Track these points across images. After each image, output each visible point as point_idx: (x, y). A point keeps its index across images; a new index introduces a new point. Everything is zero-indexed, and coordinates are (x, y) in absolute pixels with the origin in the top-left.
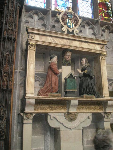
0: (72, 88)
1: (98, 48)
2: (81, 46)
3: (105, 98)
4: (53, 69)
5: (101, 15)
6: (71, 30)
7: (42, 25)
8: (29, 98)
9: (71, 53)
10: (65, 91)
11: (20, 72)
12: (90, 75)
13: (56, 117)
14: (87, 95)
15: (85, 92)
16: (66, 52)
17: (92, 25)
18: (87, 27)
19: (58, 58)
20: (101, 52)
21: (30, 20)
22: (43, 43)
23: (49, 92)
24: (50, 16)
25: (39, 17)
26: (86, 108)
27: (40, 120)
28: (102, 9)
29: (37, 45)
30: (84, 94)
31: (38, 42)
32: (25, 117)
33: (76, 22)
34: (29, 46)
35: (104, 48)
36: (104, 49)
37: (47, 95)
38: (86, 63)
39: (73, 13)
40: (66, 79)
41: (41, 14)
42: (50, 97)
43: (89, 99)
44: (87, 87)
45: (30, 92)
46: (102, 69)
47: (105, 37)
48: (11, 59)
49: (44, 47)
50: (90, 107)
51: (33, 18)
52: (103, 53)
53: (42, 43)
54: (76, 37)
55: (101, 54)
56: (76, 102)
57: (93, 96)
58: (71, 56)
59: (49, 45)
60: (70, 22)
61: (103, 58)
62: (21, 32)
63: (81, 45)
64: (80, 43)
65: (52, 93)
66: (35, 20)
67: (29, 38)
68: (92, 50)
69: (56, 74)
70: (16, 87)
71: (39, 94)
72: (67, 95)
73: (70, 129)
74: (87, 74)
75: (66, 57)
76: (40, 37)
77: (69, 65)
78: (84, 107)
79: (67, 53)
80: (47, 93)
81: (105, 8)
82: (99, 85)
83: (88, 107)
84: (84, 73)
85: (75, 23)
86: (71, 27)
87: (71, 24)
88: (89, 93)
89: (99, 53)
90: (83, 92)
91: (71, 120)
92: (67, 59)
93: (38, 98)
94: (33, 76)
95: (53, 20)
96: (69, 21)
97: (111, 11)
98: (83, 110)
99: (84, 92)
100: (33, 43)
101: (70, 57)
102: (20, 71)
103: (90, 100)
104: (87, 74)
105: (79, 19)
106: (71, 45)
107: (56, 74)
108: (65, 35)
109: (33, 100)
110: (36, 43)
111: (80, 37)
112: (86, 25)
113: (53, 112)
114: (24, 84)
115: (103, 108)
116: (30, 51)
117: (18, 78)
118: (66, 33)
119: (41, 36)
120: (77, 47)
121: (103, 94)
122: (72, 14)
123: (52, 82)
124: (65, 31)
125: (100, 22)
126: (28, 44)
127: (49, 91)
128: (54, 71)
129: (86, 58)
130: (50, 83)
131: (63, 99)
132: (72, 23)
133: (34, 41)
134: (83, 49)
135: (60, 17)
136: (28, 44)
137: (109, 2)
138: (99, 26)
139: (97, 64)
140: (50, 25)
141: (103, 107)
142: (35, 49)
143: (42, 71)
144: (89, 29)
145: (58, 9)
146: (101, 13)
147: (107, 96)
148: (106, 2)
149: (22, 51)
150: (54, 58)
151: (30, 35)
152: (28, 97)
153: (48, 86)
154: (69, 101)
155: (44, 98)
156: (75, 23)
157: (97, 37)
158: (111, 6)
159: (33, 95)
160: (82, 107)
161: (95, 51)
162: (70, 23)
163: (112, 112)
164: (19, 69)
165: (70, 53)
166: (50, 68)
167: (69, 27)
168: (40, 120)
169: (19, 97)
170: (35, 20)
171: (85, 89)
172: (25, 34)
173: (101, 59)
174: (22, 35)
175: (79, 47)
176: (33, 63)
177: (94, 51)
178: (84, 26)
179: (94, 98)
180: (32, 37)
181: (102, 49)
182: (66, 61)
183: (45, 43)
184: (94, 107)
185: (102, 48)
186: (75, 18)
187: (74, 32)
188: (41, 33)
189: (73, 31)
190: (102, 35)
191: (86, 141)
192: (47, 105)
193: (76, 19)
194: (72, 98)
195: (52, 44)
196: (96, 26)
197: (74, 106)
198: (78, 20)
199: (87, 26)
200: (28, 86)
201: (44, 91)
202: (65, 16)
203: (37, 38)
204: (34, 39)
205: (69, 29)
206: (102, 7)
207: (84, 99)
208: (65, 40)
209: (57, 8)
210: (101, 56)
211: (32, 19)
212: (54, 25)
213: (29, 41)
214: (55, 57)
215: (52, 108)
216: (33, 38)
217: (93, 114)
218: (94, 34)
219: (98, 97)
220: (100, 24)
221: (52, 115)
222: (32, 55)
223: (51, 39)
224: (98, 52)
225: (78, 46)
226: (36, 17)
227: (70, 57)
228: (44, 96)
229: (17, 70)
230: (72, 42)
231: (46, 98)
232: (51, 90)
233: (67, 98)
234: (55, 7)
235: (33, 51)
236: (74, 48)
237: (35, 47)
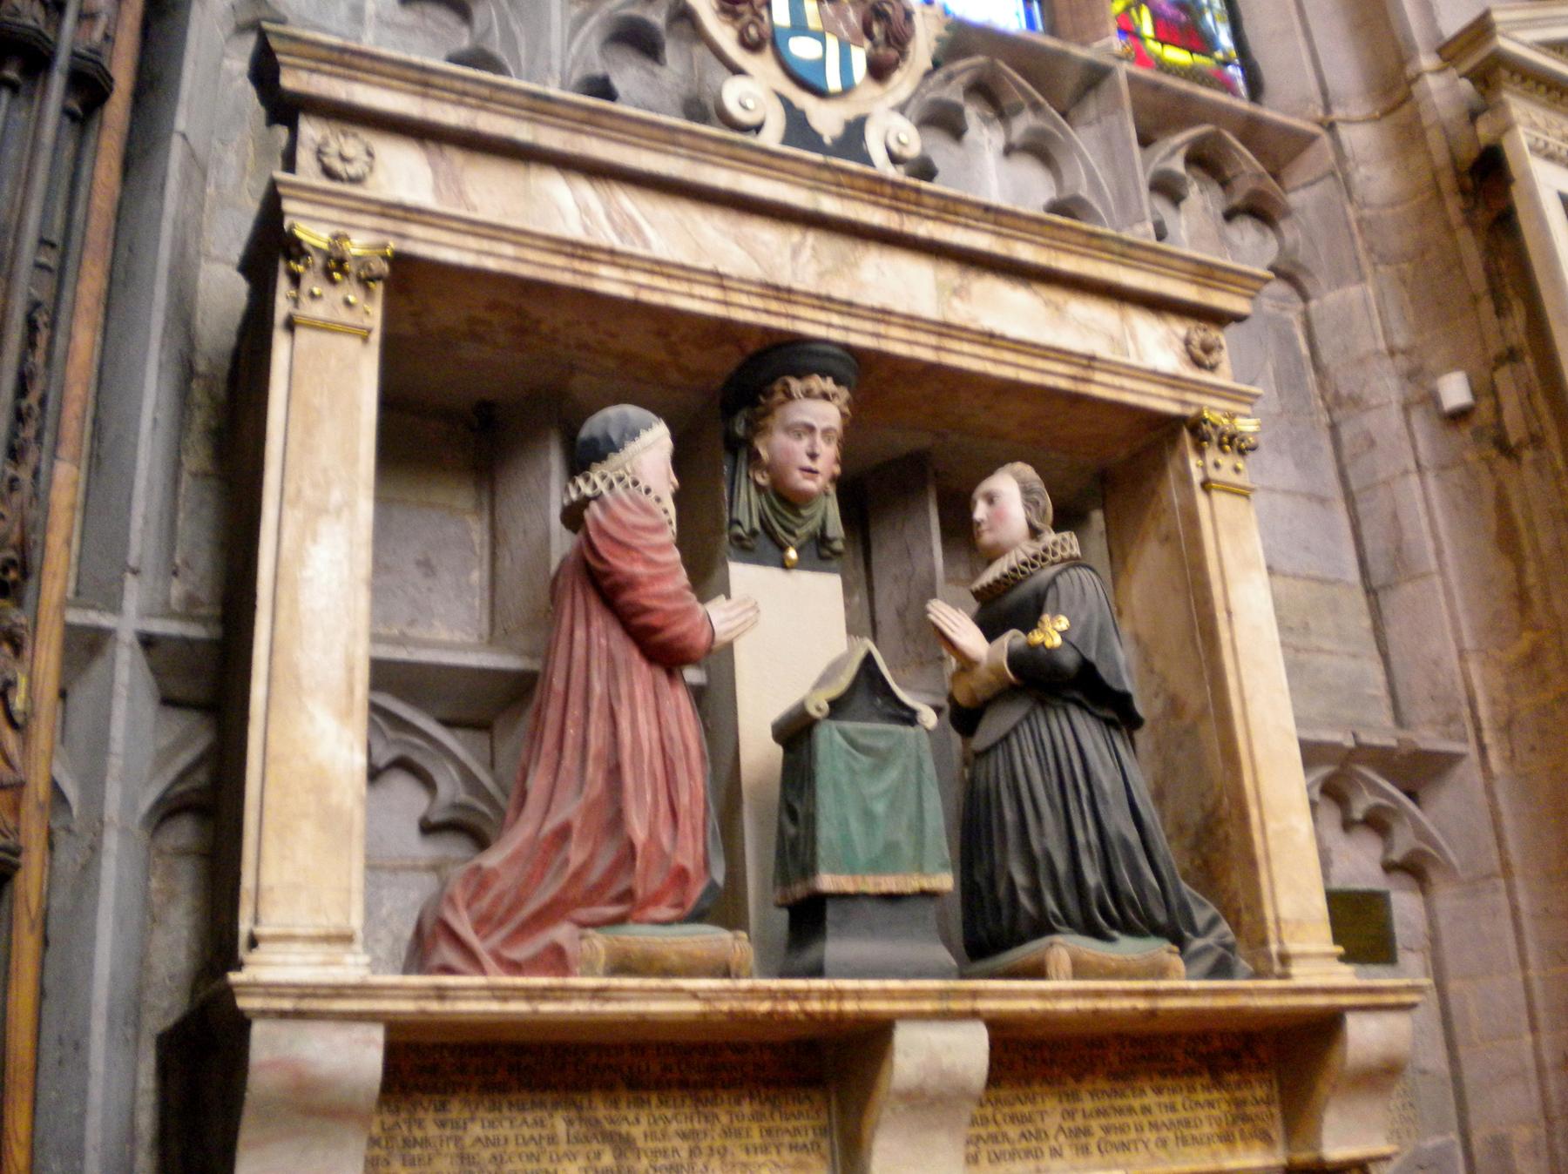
0: (891, 849)
1: (1156, 345)
2: (960, 313)
3: (1302, 975)
4: (632, 583)
6: (827, 119)
8: (299, 1015)
9: (844, 393)
10: (799, 891)
11: (148, 642)
12: (1103, 670)
14: (1090, 948)
15: (1061, 906)
16: (773, 380)
17: (1036, 107)
19: (680, 461)
23: (584, 914)
26: (1079, 1121)
29: (406, 279)
30: (1042, 927)
31: (415, 230)
34: (295, 279)
35: (1224, 358)
36: (1225, 366)
38: (1034, 533)
40: (795, 733)
42: (593, 988)
43: (1126, 1004)
44: (1080, 837)
45: (306, 923)
46: (1221, 616)
48: (23, 359)
49: (493, 306)
50: (1119, 1102)
52: (1214, 410)
53: (472, 242)
54: (903, 194)
55: (1196, 427)
56: (967, 1050)
57: (1159, 949)
58: (851, 439)
59: (560, 272)
60: (814, 22)
61: (1225, 474)
62: (181, 123)
63: (956, 302)
64: (950, 273)
65: (620, 920)
67: (290, 163)
68: (1099, 376)
69: (665, 655)
70: (95, 849)
71: (428, 943)
72: (834, 948)
74: (1069, 659)
75: (788, 453)
76: (443, 166)
77: (819, 553)
79: (789, 396)
80: (562, 933)
82: (1197, 816)
83: (1101, 1113)
84: (1034, 649)
85: (867, 44)
86: (834, 83)
89: (1174, 409)
90: (1024, 900)
92: (798, 475)
93: (434, 1006)
94: (351, 691)
99: (1051, 904)
100: (341, 230)
102: (158, 627)
103: (1142, 1004)
104: (1069, 659)
106: (840, 290)
107: (665, 655)
108: (766, 162)
109: (360, 1031)
110: (393, 245)
111: (950, 208)
112: (972, 113)
114: (209, 811)
115: (1276, 1110)
116: (302, 335)
117: (118, 730)
118: (771, 137)
120: (912, 322)
121: (1271, 924)
123: (614, 772)
126: (270, 249)
127: (590, 898)
128: (647, 610)
129: (1028, 471)
130: (596, 776)
131: (793, 1007)
132: (836, 33)
134: (989, 352)
136: (270, 249)
138: (1122, 125)
139: (1151, 559)
141: (1268, 1103)
143: (458, 636)
144: (1009, 150)
149: (188, 372)
150: (632, 447)
151: (311, 130)
152: (272, 989)
153: (563, 833)
154: (868, 1040)
155: (518, 1007)
159: (352, 967)
160: (1030, 1119)
161: (1127, 383)
162: (820, 36)
163: (1383, 1148)
164: (134, 594)
165: (825, 396)
166: (600, 582)
169: (133, 1008)
171: (1061, 865)
172: (231, 158)
173: (1206, 485)
174: (198, 167)
175: (945, 329)
176: (350, 504)
180: (338, 166)
181: (1198, 363)
182: (787, 500)
183: (509, 250)
184: (1173, 1108)
187: (862, 137)
192: (556, 1105)
195: (604, 271)
196: (1081, 130)
199: (986, 121)
200: (269, 833)
201: (507, 901)
203: (402, 172)
207: (1066, 1005)
210: (1200, 451)
213: (288, 206)
214: (646, 437)
215: (619, 1155)
216: (352, 170)
219: (1222, 968)
222: (328, 395)
223: (585, 210)
224: (1163, 402)
225: (928, 308)
227: (828, 456)
228: (515, 967)
229: (106, 621)
230: (856, 265)
231: (545, 994)
232: (619, 887)
233: (840, 995)
235: (351, 344)
236: (882, 329)
237: (368, 292)
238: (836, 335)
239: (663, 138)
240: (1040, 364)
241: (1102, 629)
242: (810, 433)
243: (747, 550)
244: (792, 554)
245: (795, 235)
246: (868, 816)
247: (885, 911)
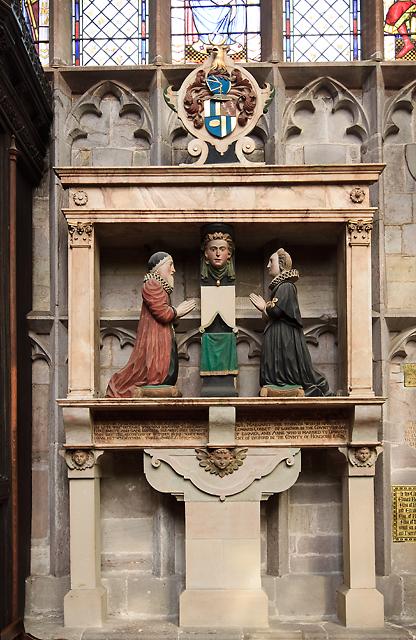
6: (222, 147)
13: (172, 462)
14: (274, 388)
20: (347, 215)
21: (89, 123)
22: (117, 216)
23: (138, 383)
27: (122, 468)
32: (352, 459)
34: (72, 235)
37: (129, 394)
38: (281, 270)
41: (127, 93)
51: (99, 115)
56: (230, 413)
57: (299, 389)
60: (218, 113)
63: (261, 200)
64: (261, 190)
66: (109, 119)
68: (311, 215)
73: (217, 499)
74: (277, 310)
76: (106, 194)
77: (227, 281)
78: (272, 429)
85: (238, 113)
86: (224, 133)
87: (224, 118)
88: (281, 379)
91: (220, 470)
96: (213, 110)
98: (267, 438)
101: (226, 251)
110: (93, 221)
113: (160, 445)
119: (108, 189)
120: (243, 211)
122: (228, 75)
133: (85, 212)
134: (271, 215)
142: (92, 244)
145: (198, 49)
147: (359, 386)
151: (72, 192)
157: (366, 142)
162: (219, 118)
167: (215, 133)
168: (122, 468)
170: (107, 123)
171: (270, 367)
177: (318, 215)
179: (299, 397)
182: (216, 268)
185: (358, 197)
186: (241, 90)
188: (105, 180)
189: (232, 147)
191: (298, 540)
194: (211, 401)
197: (223, 425)
199: (326, 100)
202: (197, 91)
203: (96, 200)
204: (84, 208)
205: (214, 142)
208: (200, 192)
211: (96, 119)
216: (82, 202)
217: (307, 453)
218: (354, 132)
221: (157, 455)
222: (83, 261)
223: (145, 198)
226: (110, 107)
228: (121, 396)
229: (52, 318)
230: (228, 196)
234: (186, 46)
236: (234, 216)
238: (219, 220)
239: (164, 172)
240: (289, 215)
241: (289, 300)
242: (220, 248)
243: (207, 283)
244: (218, 282)
245: (209, 189)
246: (216, 357)
247: (217, 379)
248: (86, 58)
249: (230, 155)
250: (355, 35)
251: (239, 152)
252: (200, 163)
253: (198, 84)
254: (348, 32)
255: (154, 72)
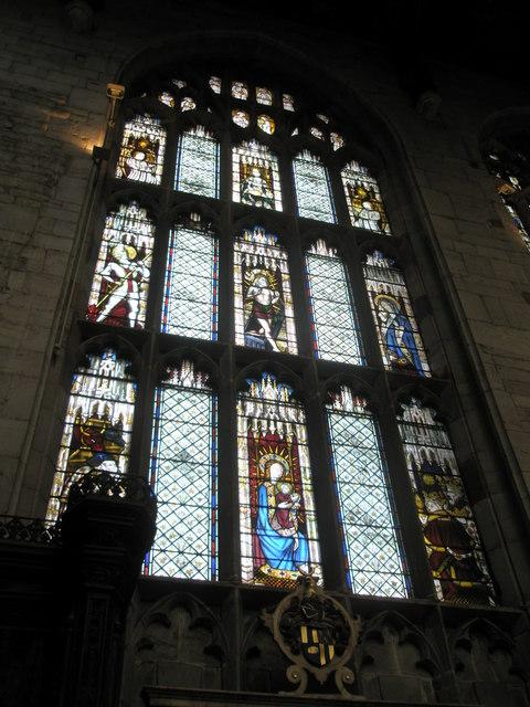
5: (445, 577)
6: (321, 675)
7: (208, 651)
18: (392, 640)
21: (157, 633)
24: (237, 609)
25: (194, 619)
28: (442, 549)
33: (340, 637)
39: (322, 600)
41: (200, 606)
47: (475, 671)
51: (167, 625)
60: (315, 640)
81: (455, 545)
86: (323, 662)
87: (322, 646)
95: (248, 625)
97: (480, 554)
105: (351, 623)
124: (299, 684)
125: (439, 609)
135: (274, 620)
137: (467, 519)
140: (238, 651)
145: (266, 572)
146: (441, 569)
148: (453, 517)
156: (335, 639)
158: (478, 532)
162: (317, 645)
170: (176, 634)
178: (377, 638)
189: (332, 676)
190: (460, 668)
193: (339, 623)
198: (349, 629)
199: (391, 632)
202: (292, 617)
205: (314, 670)
206: (440, 542)
209: (265, 570)
212: (256, 648)
218: (424, 666)
220: (442, 620)
226: (181, 619)
248: (156, 567)
249: (330, 685)
250: (213, 557)
251: (339, 684)
252: (300, 693)
253: (293, 609)
254: (206, 552)
255: (234, 589)
